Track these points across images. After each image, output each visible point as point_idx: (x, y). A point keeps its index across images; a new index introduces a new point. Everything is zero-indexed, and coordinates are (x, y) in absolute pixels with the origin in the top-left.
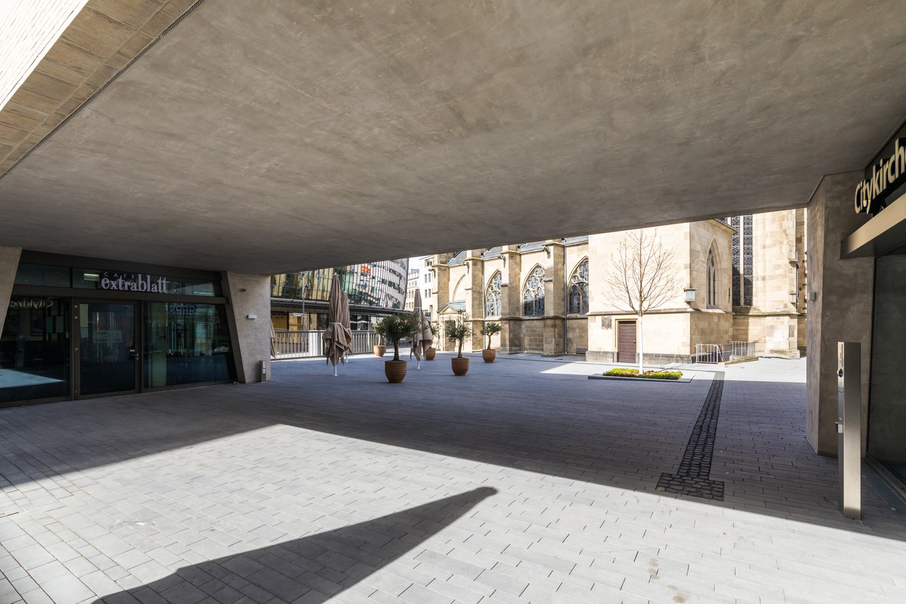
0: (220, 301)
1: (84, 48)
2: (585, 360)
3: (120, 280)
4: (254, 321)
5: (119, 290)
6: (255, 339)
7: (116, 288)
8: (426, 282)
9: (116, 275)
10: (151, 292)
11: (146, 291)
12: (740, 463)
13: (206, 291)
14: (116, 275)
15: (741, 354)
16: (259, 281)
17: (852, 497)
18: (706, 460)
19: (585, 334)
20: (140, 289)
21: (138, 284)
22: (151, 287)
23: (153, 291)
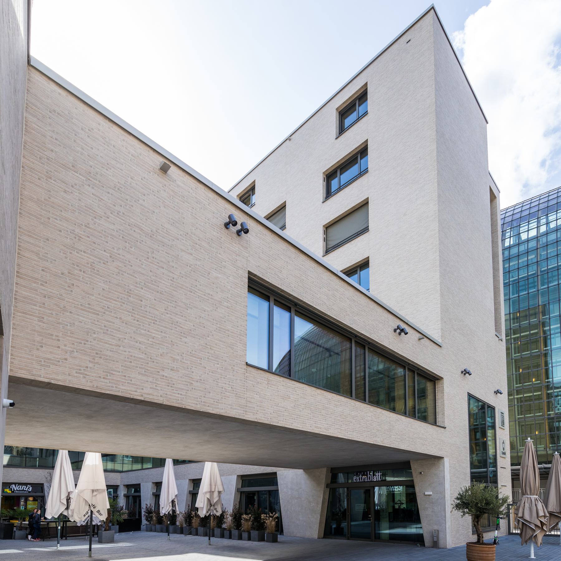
0: (334, 486)
1: (128, 395)
2: (324, 226)
3: (360, 476)
4: (431, 497)
5: (360, 482)
6: (432, 512)
7: (359, 481)
8: (504, 429)
9: (359, 474)
10: (373, 481)
11: (371, 481)
12: (178, 367)
13: (341, 478)
14: (359, 474)
15: (549, 468)
16: (434, 463)
17: (510, 398)
18: (525, 364)
19: (492, 505)
20: (369, 480)
21: (367, 477)
22: (373, 478)
23: (374, 480)
